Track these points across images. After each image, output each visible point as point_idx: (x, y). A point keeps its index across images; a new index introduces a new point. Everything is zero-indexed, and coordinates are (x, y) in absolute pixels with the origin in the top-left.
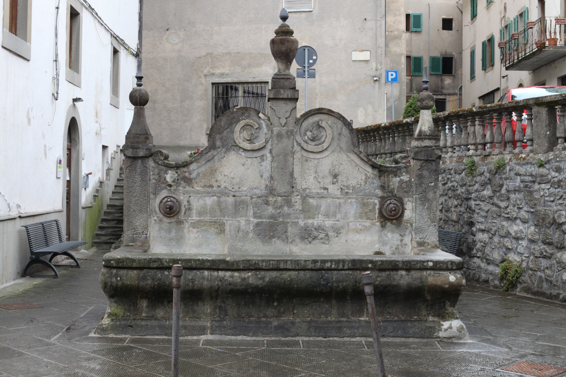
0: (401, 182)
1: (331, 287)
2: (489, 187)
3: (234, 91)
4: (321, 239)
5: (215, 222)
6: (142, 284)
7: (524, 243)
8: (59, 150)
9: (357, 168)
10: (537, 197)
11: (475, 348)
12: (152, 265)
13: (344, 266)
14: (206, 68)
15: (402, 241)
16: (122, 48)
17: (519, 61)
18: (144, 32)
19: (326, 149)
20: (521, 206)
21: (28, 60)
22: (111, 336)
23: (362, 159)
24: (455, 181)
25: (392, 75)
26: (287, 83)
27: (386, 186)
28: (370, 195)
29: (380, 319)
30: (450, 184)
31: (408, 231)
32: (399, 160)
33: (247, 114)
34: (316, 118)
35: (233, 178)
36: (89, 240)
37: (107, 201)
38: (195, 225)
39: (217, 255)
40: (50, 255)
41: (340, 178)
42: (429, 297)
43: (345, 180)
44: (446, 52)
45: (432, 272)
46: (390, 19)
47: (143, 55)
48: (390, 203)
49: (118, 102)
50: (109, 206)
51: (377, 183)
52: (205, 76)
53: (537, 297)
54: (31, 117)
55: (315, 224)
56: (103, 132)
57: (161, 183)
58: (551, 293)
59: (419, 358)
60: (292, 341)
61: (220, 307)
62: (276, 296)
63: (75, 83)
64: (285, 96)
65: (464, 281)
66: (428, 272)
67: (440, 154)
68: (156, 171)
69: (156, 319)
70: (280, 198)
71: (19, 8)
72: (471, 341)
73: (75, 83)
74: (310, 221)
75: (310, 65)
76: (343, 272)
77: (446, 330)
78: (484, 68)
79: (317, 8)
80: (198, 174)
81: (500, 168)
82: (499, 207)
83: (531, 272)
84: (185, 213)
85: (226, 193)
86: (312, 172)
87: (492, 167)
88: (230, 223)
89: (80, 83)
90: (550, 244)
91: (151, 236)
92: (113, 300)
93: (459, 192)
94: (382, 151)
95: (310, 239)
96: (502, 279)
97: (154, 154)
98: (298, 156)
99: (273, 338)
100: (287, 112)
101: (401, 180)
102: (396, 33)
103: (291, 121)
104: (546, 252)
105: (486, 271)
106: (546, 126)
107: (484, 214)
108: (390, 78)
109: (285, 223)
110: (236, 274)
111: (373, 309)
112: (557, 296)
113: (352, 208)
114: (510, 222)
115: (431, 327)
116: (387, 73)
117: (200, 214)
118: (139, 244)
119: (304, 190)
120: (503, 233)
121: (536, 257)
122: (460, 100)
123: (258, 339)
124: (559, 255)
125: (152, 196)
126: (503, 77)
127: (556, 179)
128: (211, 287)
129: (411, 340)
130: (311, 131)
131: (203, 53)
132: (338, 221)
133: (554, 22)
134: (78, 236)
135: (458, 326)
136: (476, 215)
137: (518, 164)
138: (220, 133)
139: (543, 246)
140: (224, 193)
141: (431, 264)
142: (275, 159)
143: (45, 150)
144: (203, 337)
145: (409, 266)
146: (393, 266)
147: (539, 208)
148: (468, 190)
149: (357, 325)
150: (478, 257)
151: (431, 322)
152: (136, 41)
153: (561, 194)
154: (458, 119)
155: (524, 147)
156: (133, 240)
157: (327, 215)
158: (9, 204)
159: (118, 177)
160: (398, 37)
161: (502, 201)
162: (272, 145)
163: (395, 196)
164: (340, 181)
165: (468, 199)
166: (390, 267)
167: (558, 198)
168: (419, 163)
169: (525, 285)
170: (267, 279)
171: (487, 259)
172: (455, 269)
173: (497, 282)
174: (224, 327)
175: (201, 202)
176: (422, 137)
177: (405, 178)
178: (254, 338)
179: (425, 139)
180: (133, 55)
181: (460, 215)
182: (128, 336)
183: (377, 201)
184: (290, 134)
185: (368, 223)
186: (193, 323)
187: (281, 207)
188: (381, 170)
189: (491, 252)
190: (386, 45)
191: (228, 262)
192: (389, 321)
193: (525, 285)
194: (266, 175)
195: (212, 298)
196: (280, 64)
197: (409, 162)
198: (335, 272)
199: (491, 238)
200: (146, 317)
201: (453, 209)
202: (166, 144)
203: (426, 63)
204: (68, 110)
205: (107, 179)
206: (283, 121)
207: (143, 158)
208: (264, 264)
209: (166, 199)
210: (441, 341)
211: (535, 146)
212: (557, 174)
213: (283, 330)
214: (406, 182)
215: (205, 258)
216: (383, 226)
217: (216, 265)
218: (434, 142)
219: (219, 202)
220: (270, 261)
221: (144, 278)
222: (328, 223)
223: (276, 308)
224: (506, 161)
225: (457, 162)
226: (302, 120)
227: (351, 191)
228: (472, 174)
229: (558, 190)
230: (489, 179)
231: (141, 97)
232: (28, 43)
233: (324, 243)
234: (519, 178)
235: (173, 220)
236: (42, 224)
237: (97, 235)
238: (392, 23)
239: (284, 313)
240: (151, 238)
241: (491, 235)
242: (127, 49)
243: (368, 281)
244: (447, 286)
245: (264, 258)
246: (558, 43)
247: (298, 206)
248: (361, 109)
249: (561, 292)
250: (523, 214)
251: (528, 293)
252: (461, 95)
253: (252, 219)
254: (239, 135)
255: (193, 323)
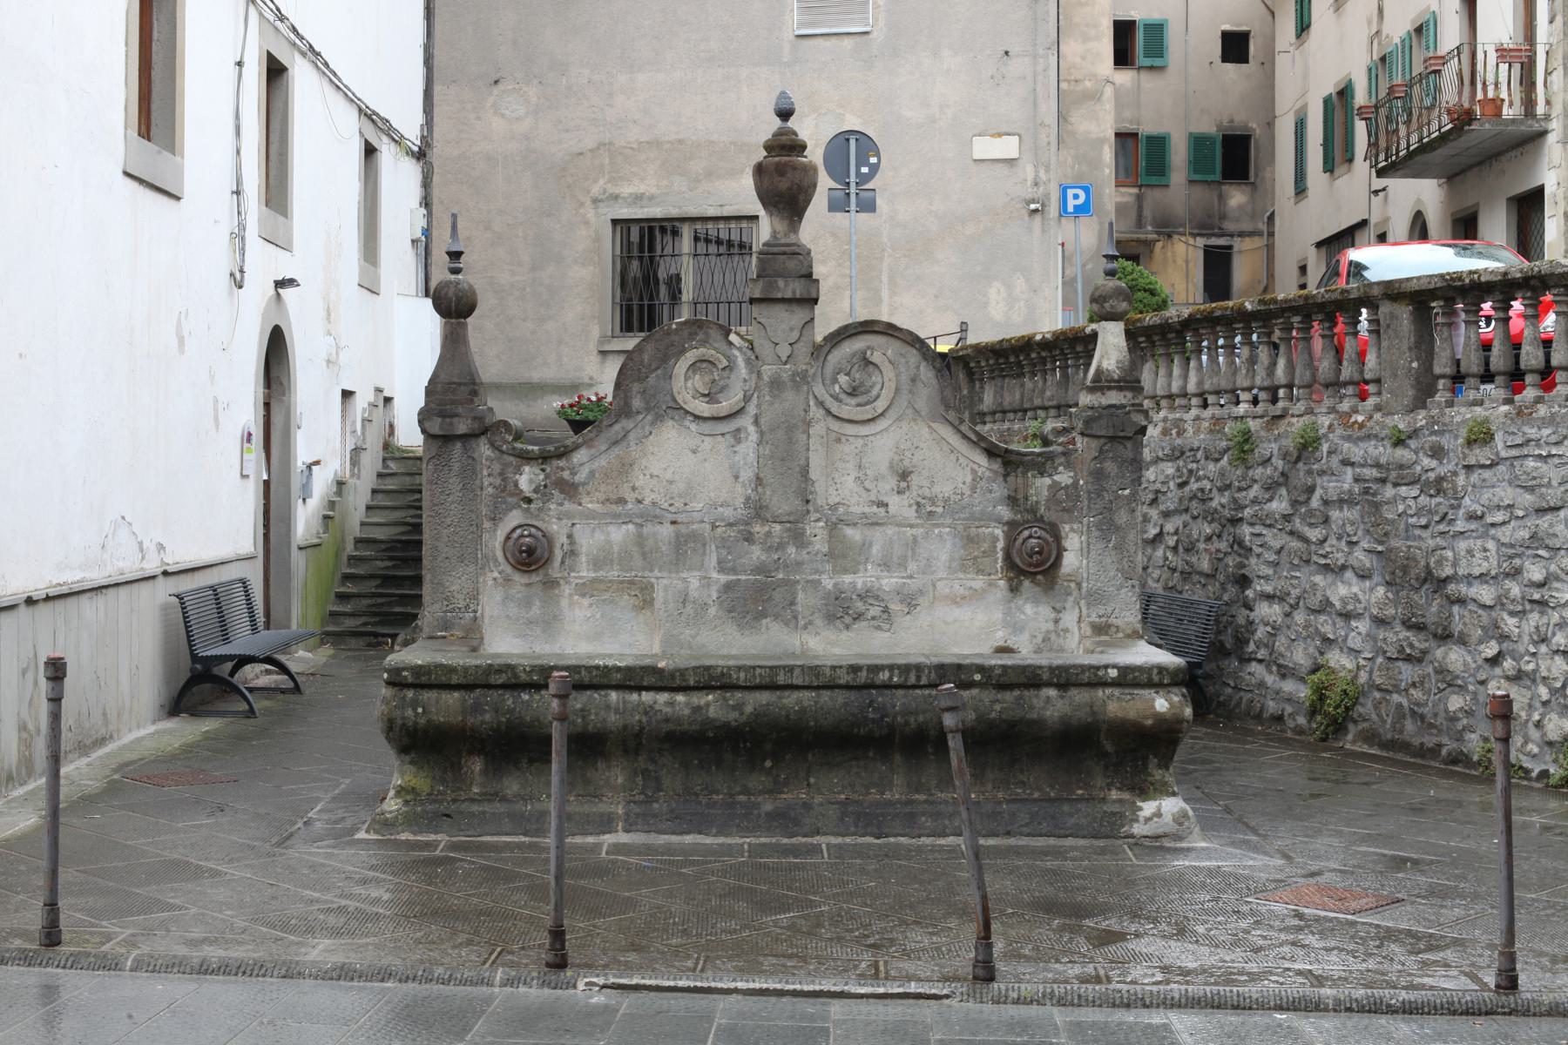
0: (1055, 487)
1: (891, 727)
2: (1283, 491)
3: (668, 238)
4: (873, 618)
5: (631, 582)
6: (471, 721)
7: (1363, 626)
8: (245, 411)
9: (953, 457)
10: (1390, 516)
11: (1210, 859)
12: (493, 679)
13: (918, 678)
14: (596, 181)
15: (1056, 621)
16: (385, 139)
17: (1411, 155)
18: (437, 89)
19: (882, 414)
20: (1355, 539)
21: (178, 199)
22: (404, 836)
23: (965, 437)
24: (1206, 477)
25: (1076, 197)
26: (792, 264)
27: (1020, 496)
28: (986, 518)
29: (1000, 795)
30: (1194, 486)
31: (1071, 599)
32: (1051, 437)
33: (701, 336)
34: (859, 344)
35: (671, 483)
36: (314, 626)
37: (354, 529)
38: (585, 589)
39: (636, 656)
40: (229, 665)
41: (915, 480)
42: (1109, 748)
43: (926, 483)
44: (1232, 121)
45: (1117, 692)
46: (1071, 48)
47: (437, 153)
48: (1030, 537)
49: (377, 279)
50: (358, 541)
51: (999, 490)
52: (595, 201)
53: (1391, 754)
54: (186, 334)
55: (859, 586)
56: (343, 357)
57: (508, 494)
58: (1422, 744)
59: (1080, 876)
60: (805, 845)
61: (645, 772)
62: (768, 747)
63: (278, 241)
64: (789, 295)
65: (1188, 711)
66: (1108, 691)
67: (1144, 423)
68: (497, 467)
69: (504, 799)
70: (777, 527)
71: (156, 74)
72: (1204, 844)
73: (278, 241)
74: (848, 579)
75: (863, 179)
76: (918, 691)
77: (1148, 820)
78: (1329, 167)
79: (881, 23)
80: (592, 473)
81: (1307, 447)
82: (1306, 540)
83: (1377, 695)
84: (563, 562)
85: (656, 517)
86: (851, 465)
87: (1289, 444)
88: (665, 585)
89: (290, 240)
90: (1420, 628)
91: (486, 615)
92: (407, 758)
93: (1214, 504)
94: (1037, 402)
95: (848, 620)
96: (1313, 712)
97: (486, 429)
98: (817, 429)
99: (763, 840)
100: (792, 329)
101: (1055, 483)
102: (1088, 84)
103: (803, 350)
104: (1411, 646)
105: (1277, 693)
106: (1410, 349)
107: (1273, 558)
108: (1071, 203)
109: (790, 584)
110: (680, 698)
111: (960, 761)
112: (1435, 751)
113: (942, 549)
114: (1330, 577)
115: (1113, 814)
116: (1064, 190)
117: (597, 564)
118: (460, 634)
119: (834, 508)
120: (1314, 602)
121: (1390, 659)
122: (1270, 248)
123: (729, 841)
124: (1439, 653)
125: (487, 525)
126: (1376, 192)
127: (1432, 475)
128: (625, 727)
129: (1070, 842)
130: (847, 374)
131: (589, 143)
132: (911, 577)
133: (1492, 57)
134: (289, 618)
135: (1176, 810)
136: (1253, 561)
137: (1349, 438)
138: (641, 380)
139: (1405, 634)
140: (651, 516)
141: (1113, 673)
142: (766, 437)
143: (216, 410)
144: (609, 839)
145: (1065, 678)
146: (1030, 679)
147: (1395, 543)
148: (1235, 500)
149: (951, 809)
150: (1260, 661)
151: (1115, 801)
152: (418, 118)
153: (1443, 509)
154: (1213, 328)
155: (1363, 396)
156: (446, 625)
157: (885, 565)
158: (141, 543)
159: (379, 467)
160: (1094, 96)
161: (1311, 525)
162: (759, 406)
163: (1041, 520)
164: (914, 487)
165: (1235, 521)
166: (1023, 680)
167: (1437, 518)
168: (1095, 444)
169: (1365, 725)
170: (749, 709)
171: (1279, 666)
172: (1168, 685)
173: (1301, 720)
174: (655, 816)
175: (599, 537)
176: (1102, 383)
177: (1064, 477)
178: (721, 840)
179: (1110, 388)
180: (410, 153)
181: (1218, 560)
182: (442, 838)
183: (999, 532)
184: (801, 380)
185: (979, 583)
186: (586, 808)
187: (781, 546)
188: (1007, 461)
189: (1288, 648)
190: (1062, 117)
191: (661, 671)
192: (1021, 801)
193: (1365, 725)
194: (747, 474)
195: (626, 752)
196: (776, 221)
197: (1073, 442)
198: (900, 692)
199: (1287, 615)
200: (481, 794)
201: (1202, 546)
202: (496, 380)
203: (1179, 154)
204: (266, 309)
205: (352, 475)
206: (784, 351)
207: (465, 438)
208: (742, 675)
209: (519, 531)
210: (1137, 843)
211: (1386, 396)
212: (1434, 463)
213: (785, 820)
214: (1067, 487)
215: (610, 663)
216: (1014, 589)
217: (635, 678)
218: (1129, 395)
219: (640, 536)
220: (754, 668)
221: (477, 708)
222: (889, 582)
223: (769, 772)
224: (1322, 431)
225: (1211, 431)
226: (826, 349)
227: (940, 510)
228: (1244, 460)
229: (1438, 500)
230: (1283, 474)
231: (459, 299)
232: (178, 158)
233: (879, 628)
234: (1349, 470)
235: (535, 578)
236: (213, 588)
237: (333, 614)
238: (1078, 60)
239: (786, 783)
240: (486, 621)
241: (1287, 608)
242: (397, 140)
243: (950, 703)
244: (1149, 722)
245: (740, 663)
246: (1505, 111)
247: (820, 545)
248: (997, 284)
249: (1445, 740)
250: (1360, 557)
251: (1371, 746)
252: (1271, 234)
253: (715, 575)
254: (685, 384)
255: (586, 808)
